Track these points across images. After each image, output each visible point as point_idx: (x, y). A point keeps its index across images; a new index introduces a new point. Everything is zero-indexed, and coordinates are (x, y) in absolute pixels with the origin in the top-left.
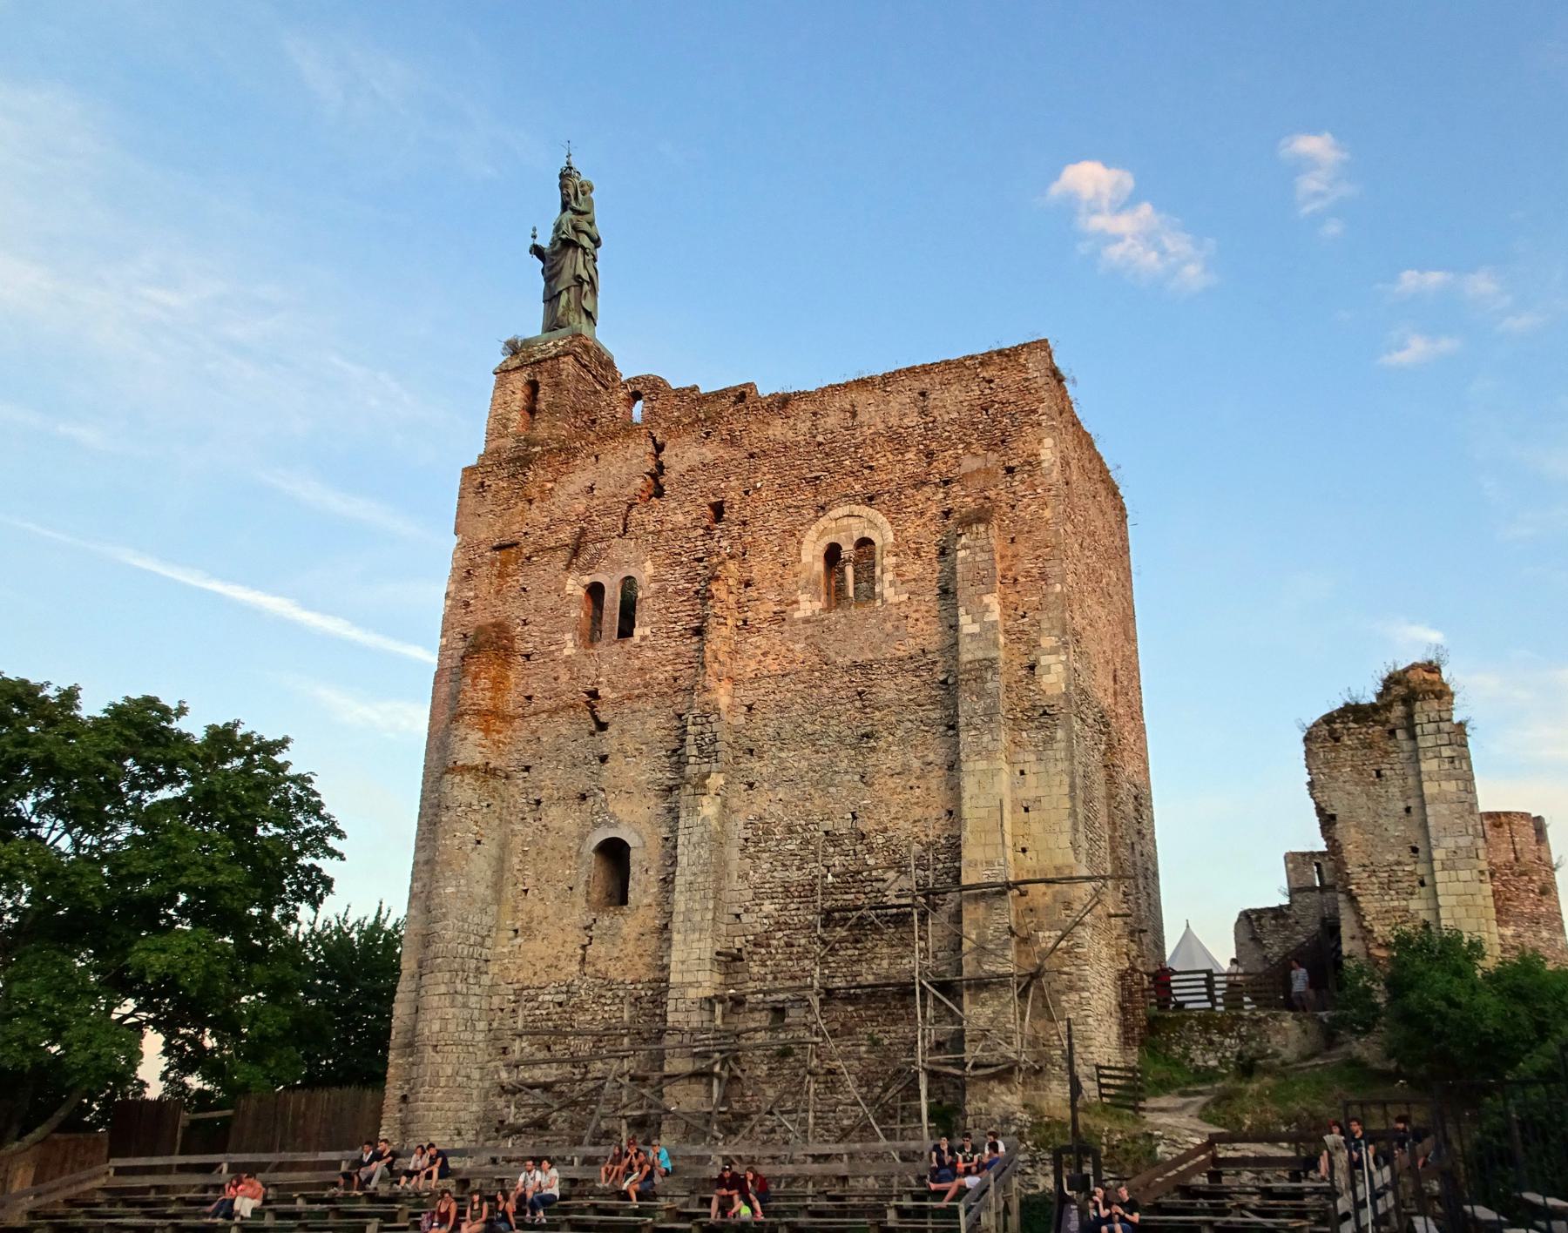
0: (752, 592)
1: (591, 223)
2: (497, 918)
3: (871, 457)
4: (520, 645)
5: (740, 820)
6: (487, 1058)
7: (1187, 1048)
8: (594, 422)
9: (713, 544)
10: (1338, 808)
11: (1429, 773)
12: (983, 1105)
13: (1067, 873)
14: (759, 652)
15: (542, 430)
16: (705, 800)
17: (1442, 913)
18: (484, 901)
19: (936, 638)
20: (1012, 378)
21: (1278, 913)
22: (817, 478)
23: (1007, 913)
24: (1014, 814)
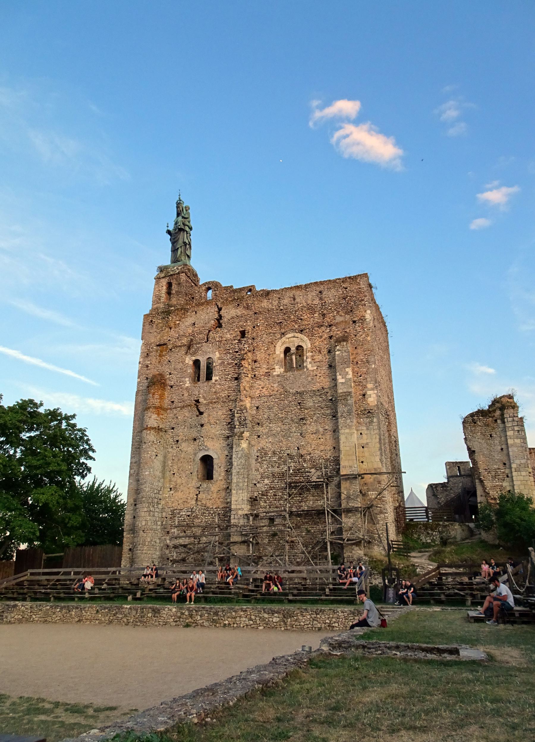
0: (257, 365)
1: (189, 222)
2: (163, 484)
3: (301, 315)
4: (168, 382)
5: (255, 449)
6: (161, 535)
7: (419, 535)
8: (193, 298)
9: (241, 346)
10: (475, 448)
11: (510, 436)
12: (350, 554)
13: (378, 471)
14: (260, 387)
15: (174, 301)
16: (242, 441)
17: (515, 487)
18: (159, 477)
19: (328, 383)
20: (355, 287)
21: (443, 485)
22: (281, 322)
23: (356, 486)
24: (357, 449)
